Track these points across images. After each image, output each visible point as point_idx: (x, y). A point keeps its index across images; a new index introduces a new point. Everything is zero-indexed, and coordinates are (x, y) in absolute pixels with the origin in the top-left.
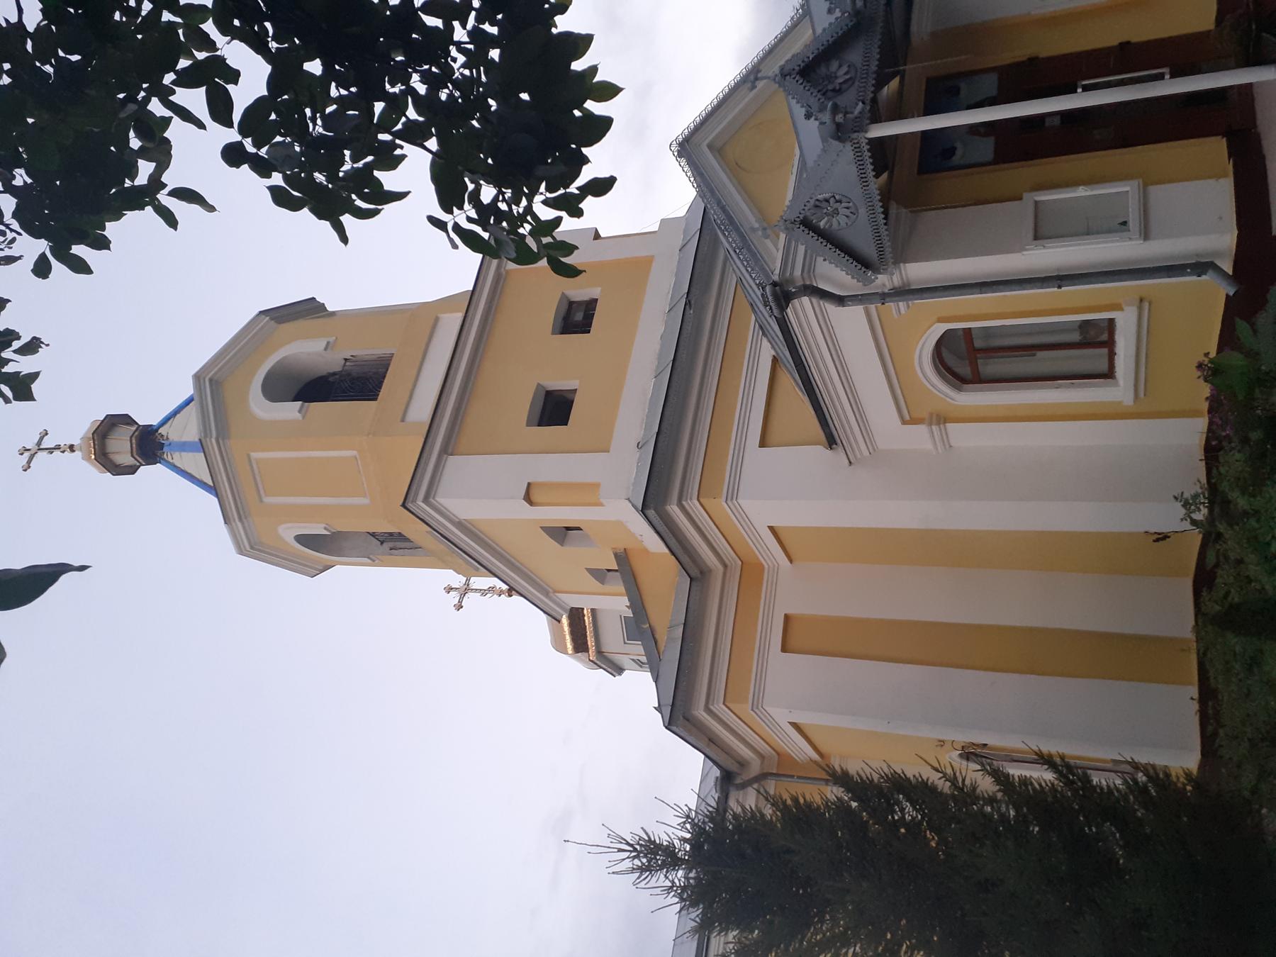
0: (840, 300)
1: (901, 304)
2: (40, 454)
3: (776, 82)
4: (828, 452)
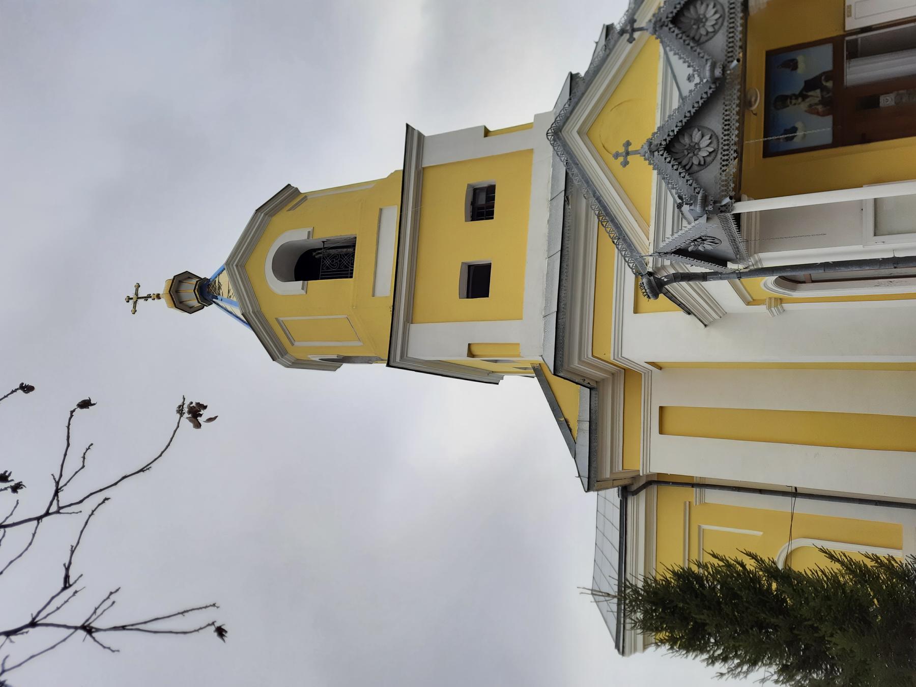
2: (140, 301)
3: (645, 159)
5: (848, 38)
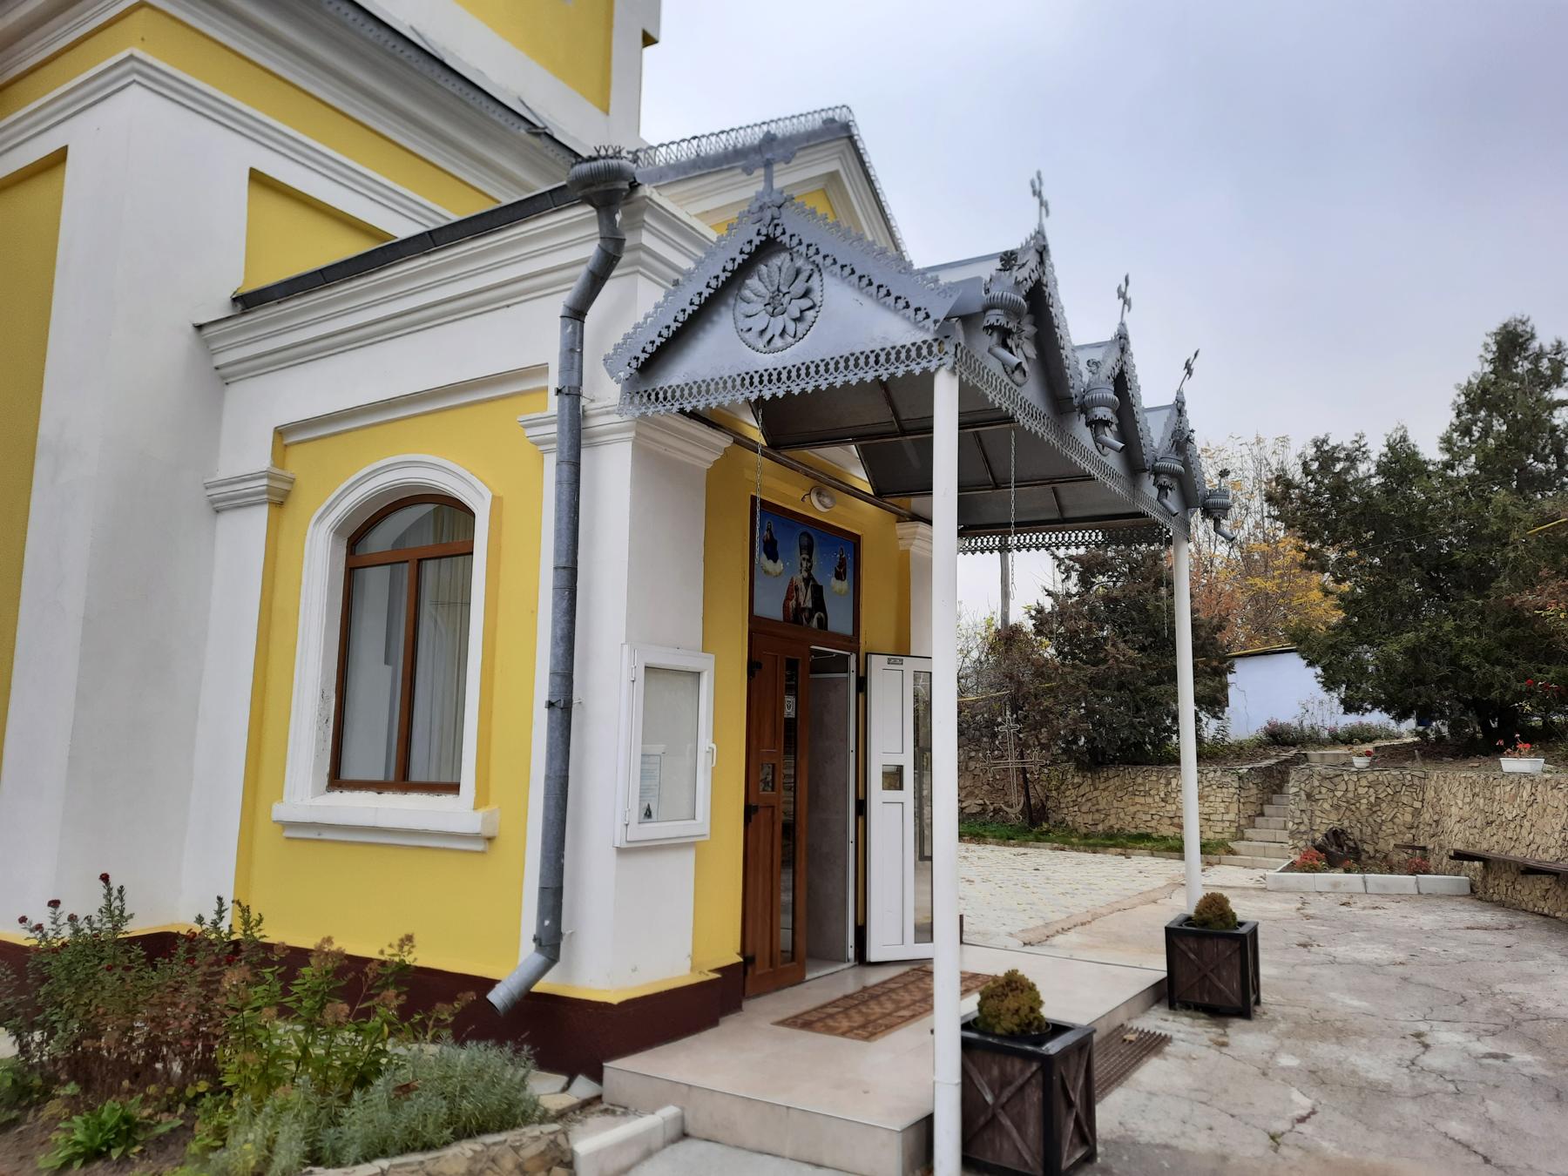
0: (577, 313)
1: (554, 428)
5: (853, 658)
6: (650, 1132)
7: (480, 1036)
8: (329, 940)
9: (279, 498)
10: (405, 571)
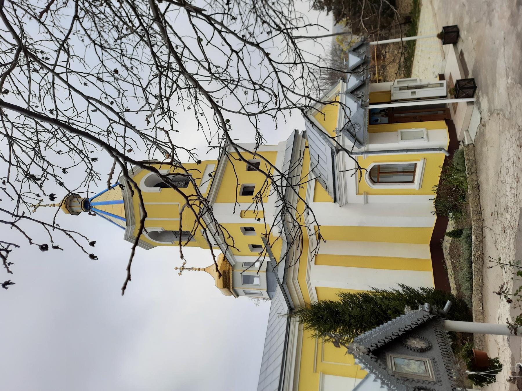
4: (334, 204)
6: (466, 135)
7: (452, 156)
8: (439, 176)
9: (367, 194)
10: (381, 175)
